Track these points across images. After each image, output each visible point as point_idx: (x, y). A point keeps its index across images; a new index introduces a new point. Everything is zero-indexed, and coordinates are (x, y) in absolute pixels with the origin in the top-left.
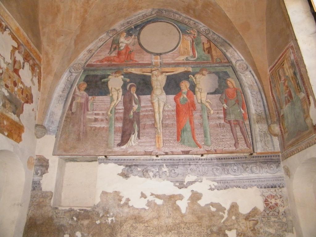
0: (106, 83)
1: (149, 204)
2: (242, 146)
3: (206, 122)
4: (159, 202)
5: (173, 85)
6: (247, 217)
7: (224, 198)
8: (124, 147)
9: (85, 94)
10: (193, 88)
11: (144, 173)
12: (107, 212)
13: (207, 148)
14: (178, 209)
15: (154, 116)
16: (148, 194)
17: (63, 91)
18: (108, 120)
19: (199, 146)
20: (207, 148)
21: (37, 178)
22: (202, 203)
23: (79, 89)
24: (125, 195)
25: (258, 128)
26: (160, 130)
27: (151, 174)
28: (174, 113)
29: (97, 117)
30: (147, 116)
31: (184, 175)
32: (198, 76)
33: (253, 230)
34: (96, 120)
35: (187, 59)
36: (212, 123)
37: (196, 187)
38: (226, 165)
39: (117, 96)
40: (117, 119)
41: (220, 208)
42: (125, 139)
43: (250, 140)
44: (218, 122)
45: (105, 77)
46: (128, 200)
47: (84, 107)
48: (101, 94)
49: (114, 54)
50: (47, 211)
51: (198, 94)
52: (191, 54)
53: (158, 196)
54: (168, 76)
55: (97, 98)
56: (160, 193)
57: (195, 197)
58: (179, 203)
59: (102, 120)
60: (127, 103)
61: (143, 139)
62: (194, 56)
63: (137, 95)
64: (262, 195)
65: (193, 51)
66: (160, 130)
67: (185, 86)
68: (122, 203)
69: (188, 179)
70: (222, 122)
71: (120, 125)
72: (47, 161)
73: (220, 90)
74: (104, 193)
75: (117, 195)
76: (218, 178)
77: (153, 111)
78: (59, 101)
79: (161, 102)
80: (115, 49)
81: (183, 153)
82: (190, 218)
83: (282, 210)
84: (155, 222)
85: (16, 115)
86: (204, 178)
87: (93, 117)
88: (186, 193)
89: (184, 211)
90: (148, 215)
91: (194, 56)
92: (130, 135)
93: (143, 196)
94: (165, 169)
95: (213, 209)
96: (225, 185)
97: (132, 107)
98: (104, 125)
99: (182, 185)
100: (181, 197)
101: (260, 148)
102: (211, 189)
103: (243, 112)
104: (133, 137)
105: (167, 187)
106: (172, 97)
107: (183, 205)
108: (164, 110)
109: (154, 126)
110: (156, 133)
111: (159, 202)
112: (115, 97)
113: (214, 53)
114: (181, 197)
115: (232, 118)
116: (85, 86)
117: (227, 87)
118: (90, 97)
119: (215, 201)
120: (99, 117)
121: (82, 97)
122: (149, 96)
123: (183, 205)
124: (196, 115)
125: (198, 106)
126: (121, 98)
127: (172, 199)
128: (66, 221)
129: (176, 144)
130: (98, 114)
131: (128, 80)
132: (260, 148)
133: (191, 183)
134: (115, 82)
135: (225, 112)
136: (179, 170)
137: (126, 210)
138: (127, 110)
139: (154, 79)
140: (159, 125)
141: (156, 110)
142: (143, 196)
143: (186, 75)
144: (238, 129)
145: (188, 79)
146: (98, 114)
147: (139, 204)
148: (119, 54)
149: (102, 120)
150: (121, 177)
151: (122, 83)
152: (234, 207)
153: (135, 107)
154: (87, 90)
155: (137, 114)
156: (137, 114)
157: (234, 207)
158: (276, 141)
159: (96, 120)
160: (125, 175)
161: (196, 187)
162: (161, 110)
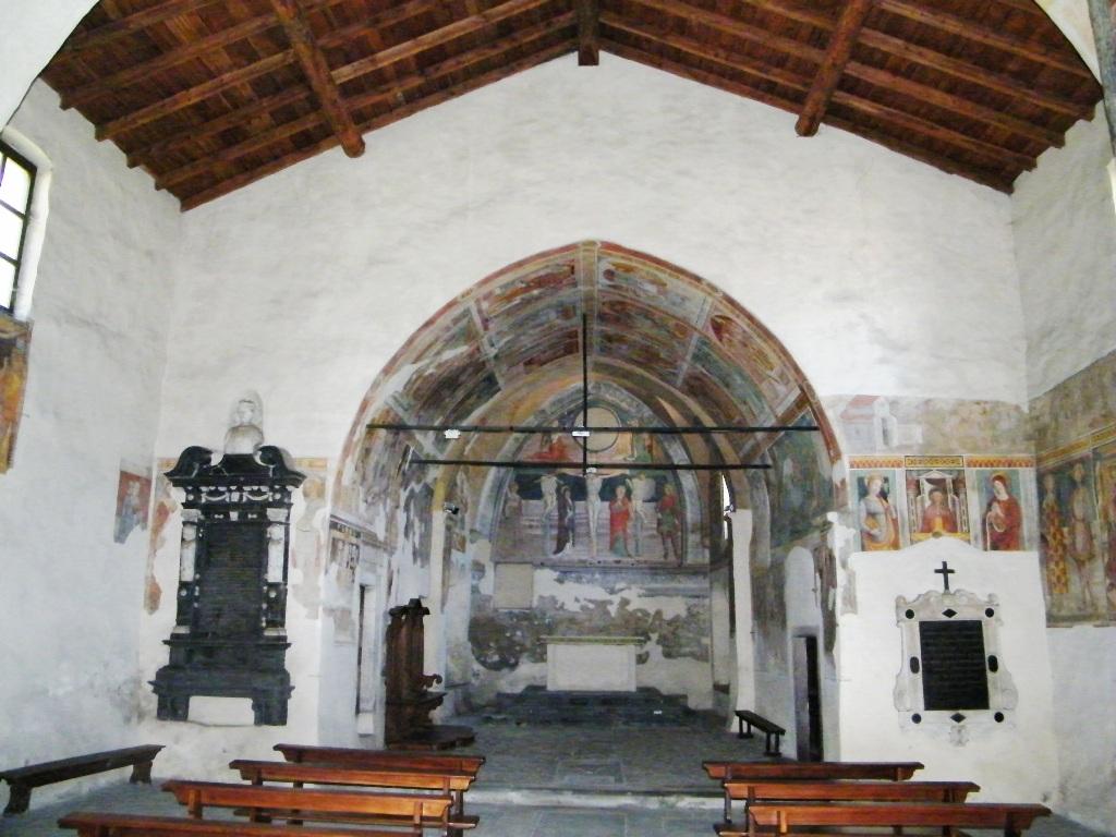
0: (539, 486)
1: (583, 608)
2: (672, 558)
3: (639, 533)
4: (591, 606)
5: (608, 491)
6: (670, 623)
7: (650, 605)
8: (560, 555)
9: (517, 497)
10: (629, 493)
11: (578, 580)
12: (545, 614)
13: (637, 558)
14: (608, 613)
15: (588, 525)
16: (581, 599)
17: (492, 491)
18: (544, 527)
19: (629, 556)
20: (637, 558)
21: (475, 582)
22: (630, 608)
23: (511, 491)
24: (561, 599)
25: (693, 539)
26: (595, 540)
27: (584, 580)
28: (608, 522)
29: (532, 523)
30: (581, 524)
31: (615, 583)
32: (635, 480)
33: (673, 633)
34: (531, 527)
35: (625, 459)
36: (645, 533)
37: (625, 594)
38: (656, 574)
39: (551, 500)
40: (551, 526)
41: (646, 614)
42: (560, 548)
43: (679, 552)
44: (651, 532)
45: (538, 477)
46: (563, 604)
47: (518, 511)
48: (533, 498)
49: (546, 450)
50: (489, 612)
51: (634, 502)
52: (630, 452)
53: (590, 601)
54: (604, 480)
55: (531, 501)
56: (593, 598)
57: (625, 602)
58: (610, 608)
59: (537, 527)
60: (562, 507)
61: (578, 547)
62: (632, 456)
63: (572, 500)
64: (686, 604)
65: (632, 450)
66: (595, 540)
67: (621, 491)
68: (557, 606)
69: (618, 586)
70: (655, 532)
71: (555, 532)
72: (483, 566)
73: (657, 497)
74: (541, 597)
75: (553, 599)
76: (646, 586)
77: (587, 518)
78: (249, 402)
79: (596, 510)
80: (547, 441)
81: (837, 828)
82: (618, 622)
83: (702, 617)
84: (587, 624)
85: (216, 460)
86: (633, 587)
87: (527, 523)
88: (616, 599)
89: (613, 615)
90: (582, 617)
91: (632, 456)
92: (564, 545)
93: (577, 600)
94: (597, 576)
95: (639, 614)
96: (652, 593)
97: (566, 513)
98: (539, 532)
99: (612, 592)
100: (611, 603)
101: (690, 559)
102: (640, 596)
103: (677, 522)
104: (568, 545)
105: (599, 593)
106: (607, 504)
107: (613, 610)
108: (598, 518)
109: (588, 534)
110: (591, 542)
111: (591, 606)
112: (549, 502)
113: (654, 452)
114: (611, 603)
115: (665, 528)
116: (517, 487)
117: (665, 494)
118: (523, 502)
119: (642, 607)
120: (534, 524)
121: (515, 500)
122: (583, 502)
123: (613, 610)
124: (630, 524)
125: (632, 515)
126: (555, 503)
127: (603, 604)
128: (507, 622)
129: (609, 554)
130: (533, 520)
131: (562, 482)
132: (690, 559)
133: (622, 590)
134: (549, 484)
135: (660, 523)
136: (611, 578)
137: (561, 612)
138: (562, 516)
139: (589, 482)
140: (593, 534)
141: (591, 519)
142: (577, 600)
143: (621, 480)
144: (669, 541)
145: (624, 483)
146: (533, 520)
147: (572, 607)
148: (551, 449)
149: (537, 527)
150: (557, 583)
151: (555, 486)
152: (659, 613)
153: (570, 514)
154: (518, 492)
155: (572, 520)
156: (572, 520)
157: (659, 613)
158: (707, 553)
159: (531, 527)
160: (560, 581)
161: (625, 594)
162: (596, 517)
